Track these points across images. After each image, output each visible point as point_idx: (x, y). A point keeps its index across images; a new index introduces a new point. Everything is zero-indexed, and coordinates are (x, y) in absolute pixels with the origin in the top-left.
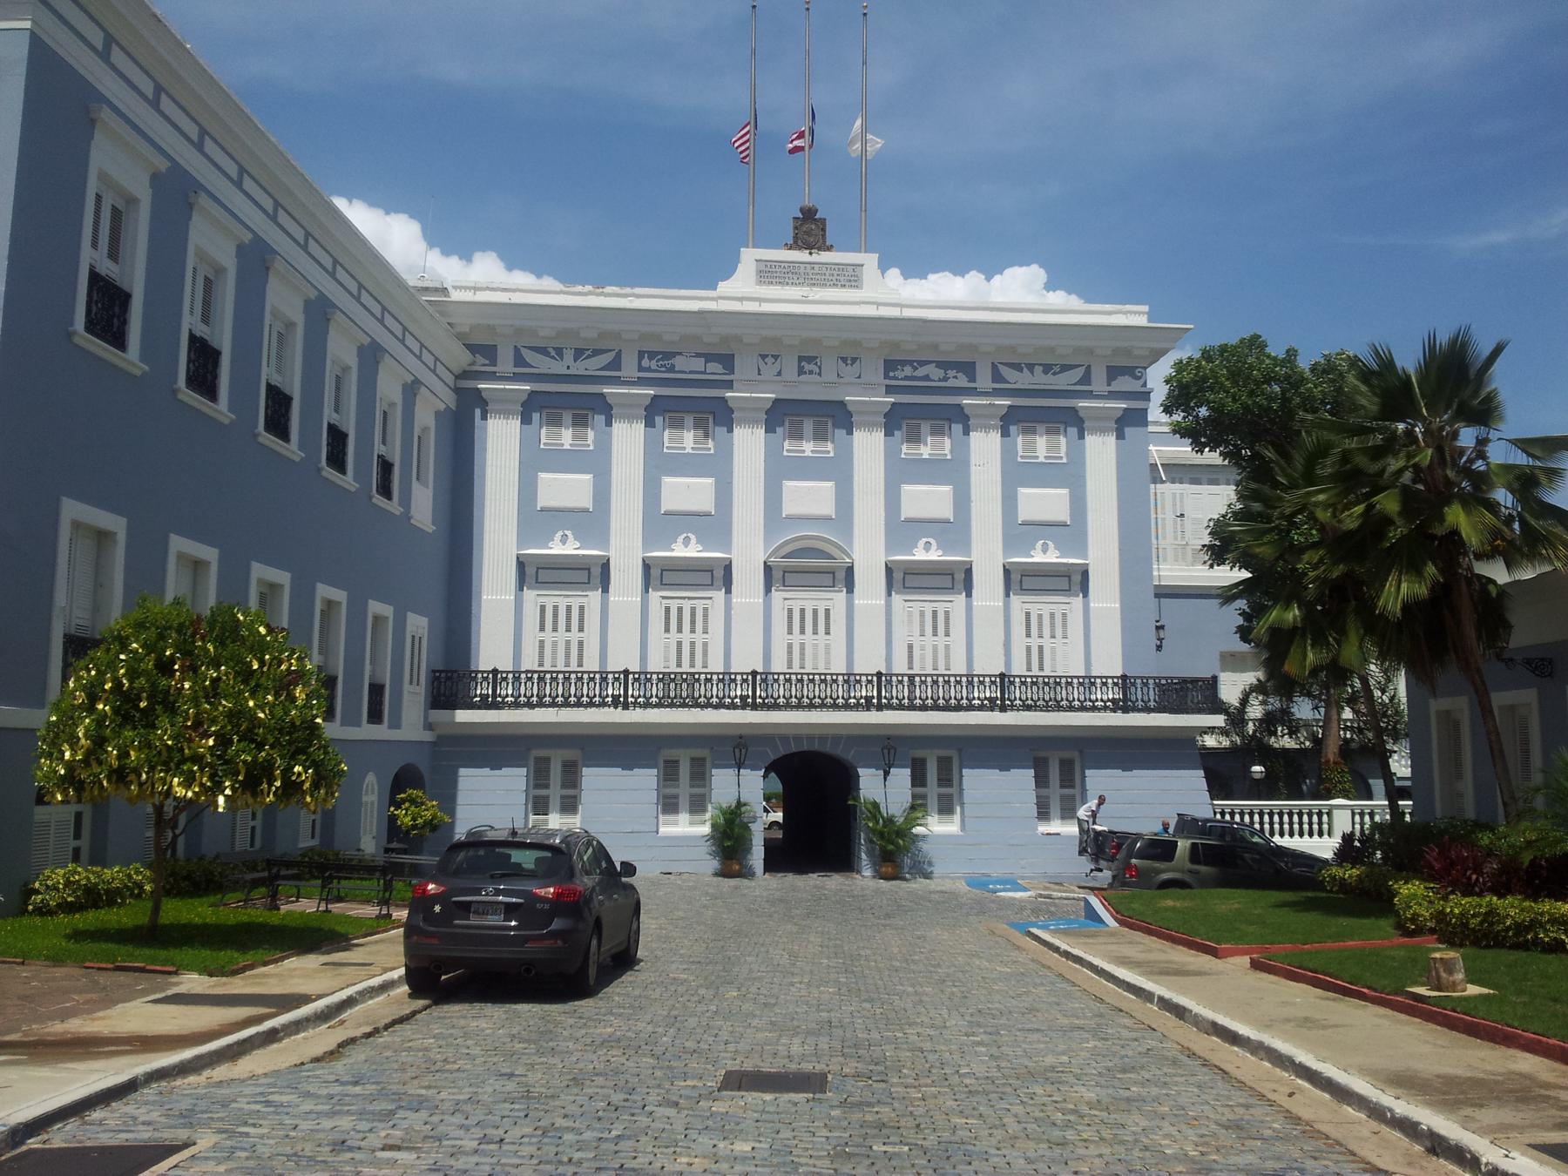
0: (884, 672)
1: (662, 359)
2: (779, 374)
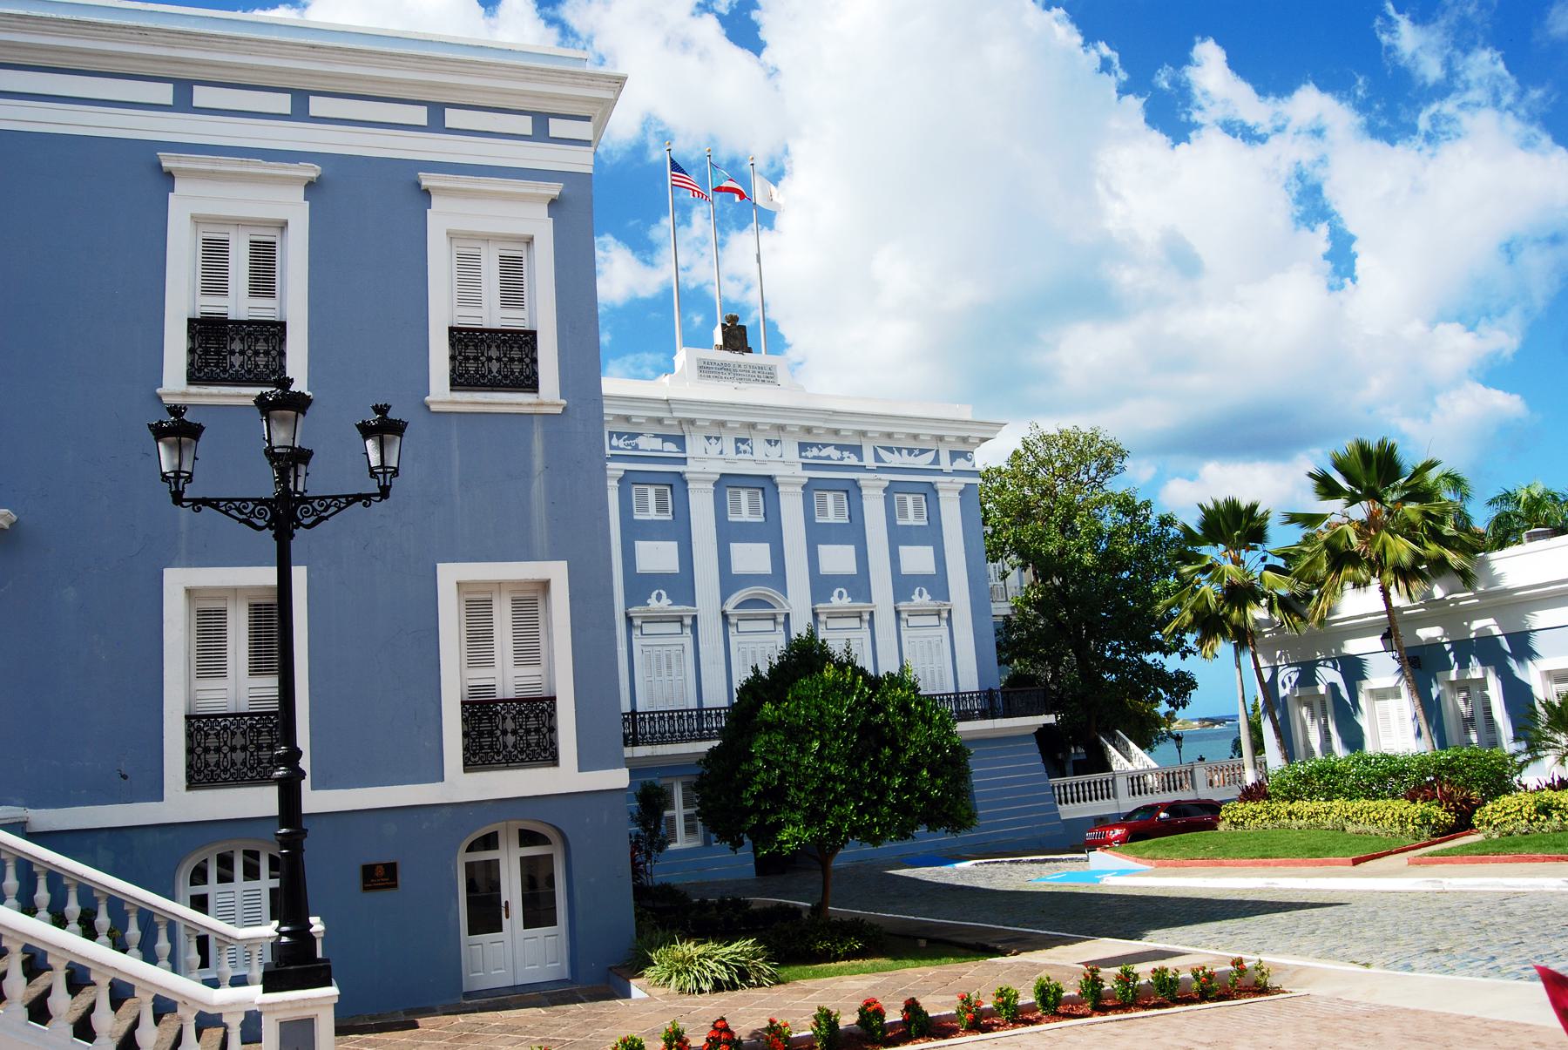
1: (628, 439)
2: (721, 453)
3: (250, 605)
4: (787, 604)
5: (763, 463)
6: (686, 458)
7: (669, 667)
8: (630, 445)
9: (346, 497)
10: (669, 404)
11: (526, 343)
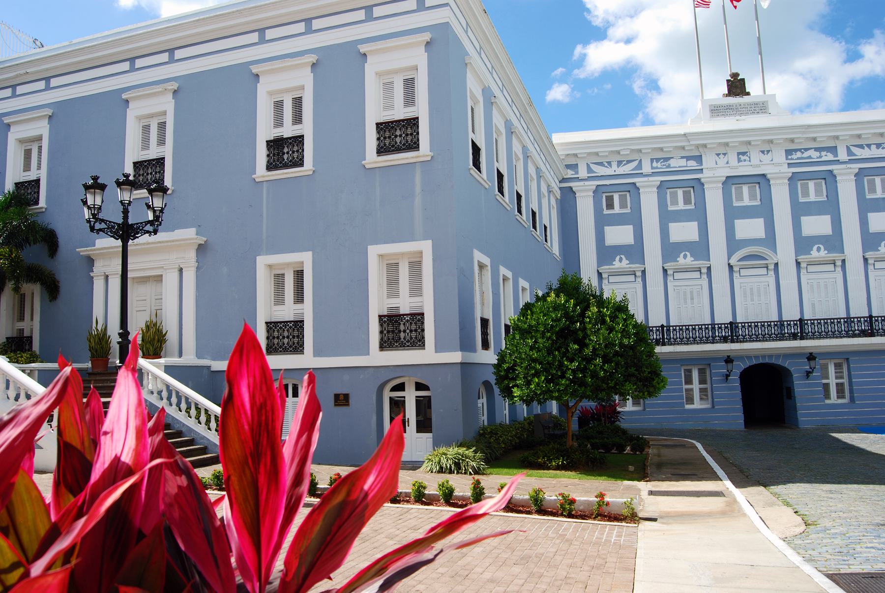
0: (665, 325)
1: (663, 162)
2: (727, 163)
3: (294, 271)
4: (777, 258)
5: (758, 166)
6: (702, 169)
7: (692, 299)
8: (665, 165)
9: (145, 222)
10: (687, 137)
11: (414, 124)
